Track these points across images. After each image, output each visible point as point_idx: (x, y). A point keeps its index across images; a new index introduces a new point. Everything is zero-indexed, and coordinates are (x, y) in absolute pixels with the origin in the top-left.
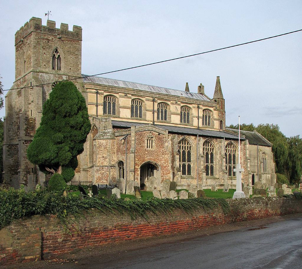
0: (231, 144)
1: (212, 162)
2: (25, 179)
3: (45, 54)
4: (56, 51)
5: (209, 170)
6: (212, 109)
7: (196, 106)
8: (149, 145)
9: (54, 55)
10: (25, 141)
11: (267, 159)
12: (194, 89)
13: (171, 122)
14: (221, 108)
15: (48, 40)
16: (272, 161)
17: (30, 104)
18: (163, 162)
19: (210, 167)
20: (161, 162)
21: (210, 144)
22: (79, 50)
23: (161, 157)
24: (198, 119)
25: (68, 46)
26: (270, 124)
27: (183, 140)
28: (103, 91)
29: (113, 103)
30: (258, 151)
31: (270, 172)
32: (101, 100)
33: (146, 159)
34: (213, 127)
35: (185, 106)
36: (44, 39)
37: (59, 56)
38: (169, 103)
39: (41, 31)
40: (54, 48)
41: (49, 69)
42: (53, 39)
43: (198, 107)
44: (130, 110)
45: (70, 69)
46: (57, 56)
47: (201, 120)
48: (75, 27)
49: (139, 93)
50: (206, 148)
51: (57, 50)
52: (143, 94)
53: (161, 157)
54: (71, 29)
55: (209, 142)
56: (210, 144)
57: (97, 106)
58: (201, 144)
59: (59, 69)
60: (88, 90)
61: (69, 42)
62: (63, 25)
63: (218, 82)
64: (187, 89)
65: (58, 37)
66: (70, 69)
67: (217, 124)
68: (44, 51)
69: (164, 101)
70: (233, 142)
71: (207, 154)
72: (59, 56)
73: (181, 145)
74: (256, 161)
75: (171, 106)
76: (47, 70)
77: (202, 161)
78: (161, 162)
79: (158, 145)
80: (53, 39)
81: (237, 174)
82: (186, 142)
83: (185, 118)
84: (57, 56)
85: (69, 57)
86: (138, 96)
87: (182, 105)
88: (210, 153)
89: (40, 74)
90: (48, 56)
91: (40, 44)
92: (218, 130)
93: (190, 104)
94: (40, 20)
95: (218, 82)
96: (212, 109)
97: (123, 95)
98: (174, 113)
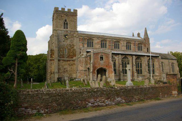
0: (126, 57)
1: (141, 67)
2: (50, 76)
4: (66, 21)
9: (65, 23)
10: (50, 60)
11: (174, 66)
12: (136, 35)
15: (62, 16)
16: (177, 67)
17: (53, 44)
21: (139, 59)
22: (76, 20)
25: (71, 18)
26: (8, 30)
27: (124, 57)
37: (67, 23)
40: (64, 19)
41: (62, 29)
46: (66, 23)
48: (74, 10)
50: (125, 60)
51: (66, 20)
54: (72, 11)
55: (139, 58)
56: (139, 59)
59: (67, 28)
62: (62, 9)
64: (133, 36)
65: (66, 14)
72: (67, 23)
73: (124, 60)
74: (168, 67)
76: (61, 29)
81: (128, 71)
82: (127, 58)
83: (140, 48)
84: (66, 23)
88: (140, 63)
90: (62, 22)
94: (58, 8)
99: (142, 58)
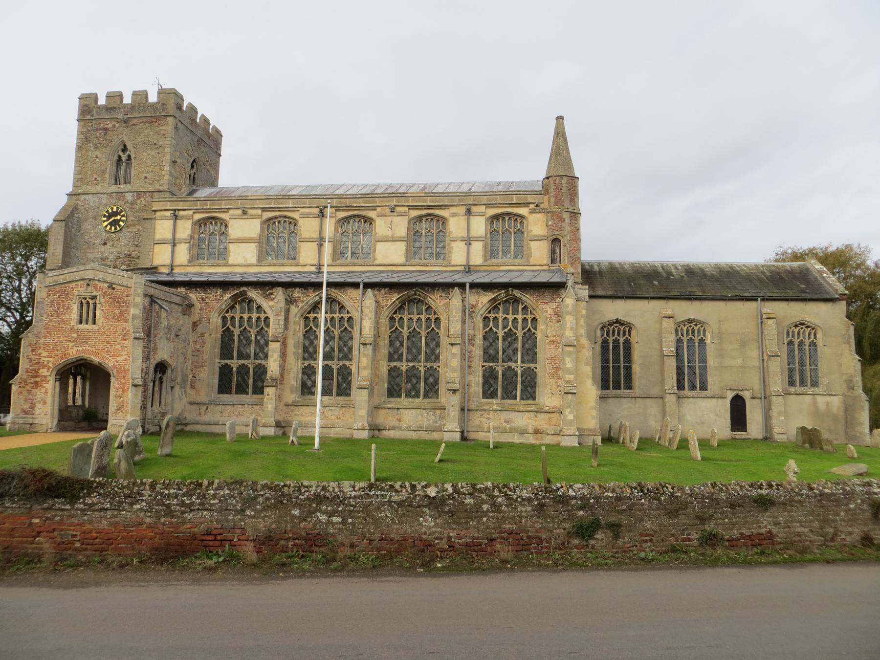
3: (97, 157)
4: (125, 149)
5: (410, 381)
6: (523, 211)
7: (463, 210)
8: (84, 316)
9: (120, 157)
13: (377, 262)
14: (556, 204)
18: (123, 358)
19: (235, 369)
20: (118, 359)
23: (117, 347)
24: (321, 245)
28: (191, 212)
29: (515, 233)
30: (761, 320)
31: (840, 387)
32: (185, 229)
33: (70, 351)
34: (528, 261)
35: (280, 216)
36: (97, 130)
37: (129, 156)
38: (372, 214)
39: (92, 116)
42: (114, 126)
43: (469, 212)
44: (481, 243)
45: (146, 178)
47: (328, 248)
49: (282, 203)
52: (459, 200)
53: (117, 347)
57: (174, 245)
58: (368, 308)
60: (158, 214)
61: (146, 125)
63: (560, 134)
66: (146, 178)
67: (539, 252)
68: (97, 153)
69: (356, 213)
70: (517, 293)
71: (791, 343)
75: (301, 222)
77: (366, 356)
78: (118, 359)
79: (111, 315)
80: (114, 126)
85: (145, 154)
86: (279, 209)
87: (415, 213)
89: (83, 197)
91: (90, 142)
92: (546, 268)
93: (440, 207)
95: (560, 134)
96: (523, 211)
97: (239, 212)
98: (387, 237)
99: (436, 300)
